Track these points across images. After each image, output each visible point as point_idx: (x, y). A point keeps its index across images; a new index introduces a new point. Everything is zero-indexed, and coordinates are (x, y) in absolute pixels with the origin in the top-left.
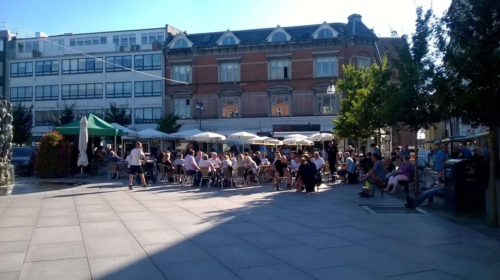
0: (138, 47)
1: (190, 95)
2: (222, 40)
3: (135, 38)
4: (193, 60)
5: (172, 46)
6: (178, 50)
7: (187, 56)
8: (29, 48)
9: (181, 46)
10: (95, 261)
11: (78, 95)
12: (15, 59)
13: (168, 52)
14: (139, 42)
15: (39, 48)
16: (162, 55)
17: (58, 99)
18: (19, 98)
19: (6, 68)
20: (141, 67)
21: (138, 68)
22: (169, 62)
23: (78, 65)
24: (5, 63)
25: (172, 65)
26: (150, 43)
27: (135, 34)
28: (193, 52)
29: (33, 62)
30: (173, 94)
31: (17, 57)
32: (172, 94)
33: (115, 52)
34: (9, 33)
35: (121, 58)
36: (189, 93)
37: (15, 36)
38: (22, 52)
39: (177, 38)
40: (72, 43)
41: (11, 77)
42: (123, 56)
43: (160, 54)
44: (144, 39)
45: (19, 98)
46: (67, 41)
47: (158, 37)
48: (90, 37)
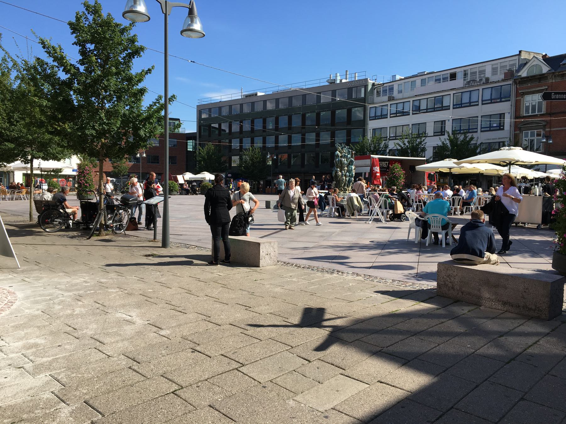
0: (487, 79)
1: (542, 126)
2: (527, 70)
3: (485, 70)
4: (548, 87)
5: (524, 73)
6: (530, 78)
7: (541, 83)
8: (385, 93)
9: (535, 72)
10: (189, 292)
11: (469, 129)
12: (373, 103)
13: (519, 81)
14: (488, 74)
15: (486, 73)
16: (513, 85)
17: (477, 132)
18: (462, 130)
19: (366, 113)
20: (398, 114)
21: (456, 106)
22: (520, 92)
23: (427, 104)
24: (365, 109)
25: (524, 94)
26: (501, 74)
27: (393, 85)
28: (549, 78)
29: (450, 94)
30: (523, 126)
31: (375, 101)
32: (521, 126)
33: (463, 87)
34: (369, 81)
35: (434, 98)
36: (541, 124)
37: (374, 82)
38: (380, 96)
39: (531, 64)
40: (423, 82)
41: (370, 120)
42: (435, 97)
43: (511, 84)
44: (494, 71)
45: (462, 130)
46: (418, 81)
47: (480, 72)
48: (497, 64)
